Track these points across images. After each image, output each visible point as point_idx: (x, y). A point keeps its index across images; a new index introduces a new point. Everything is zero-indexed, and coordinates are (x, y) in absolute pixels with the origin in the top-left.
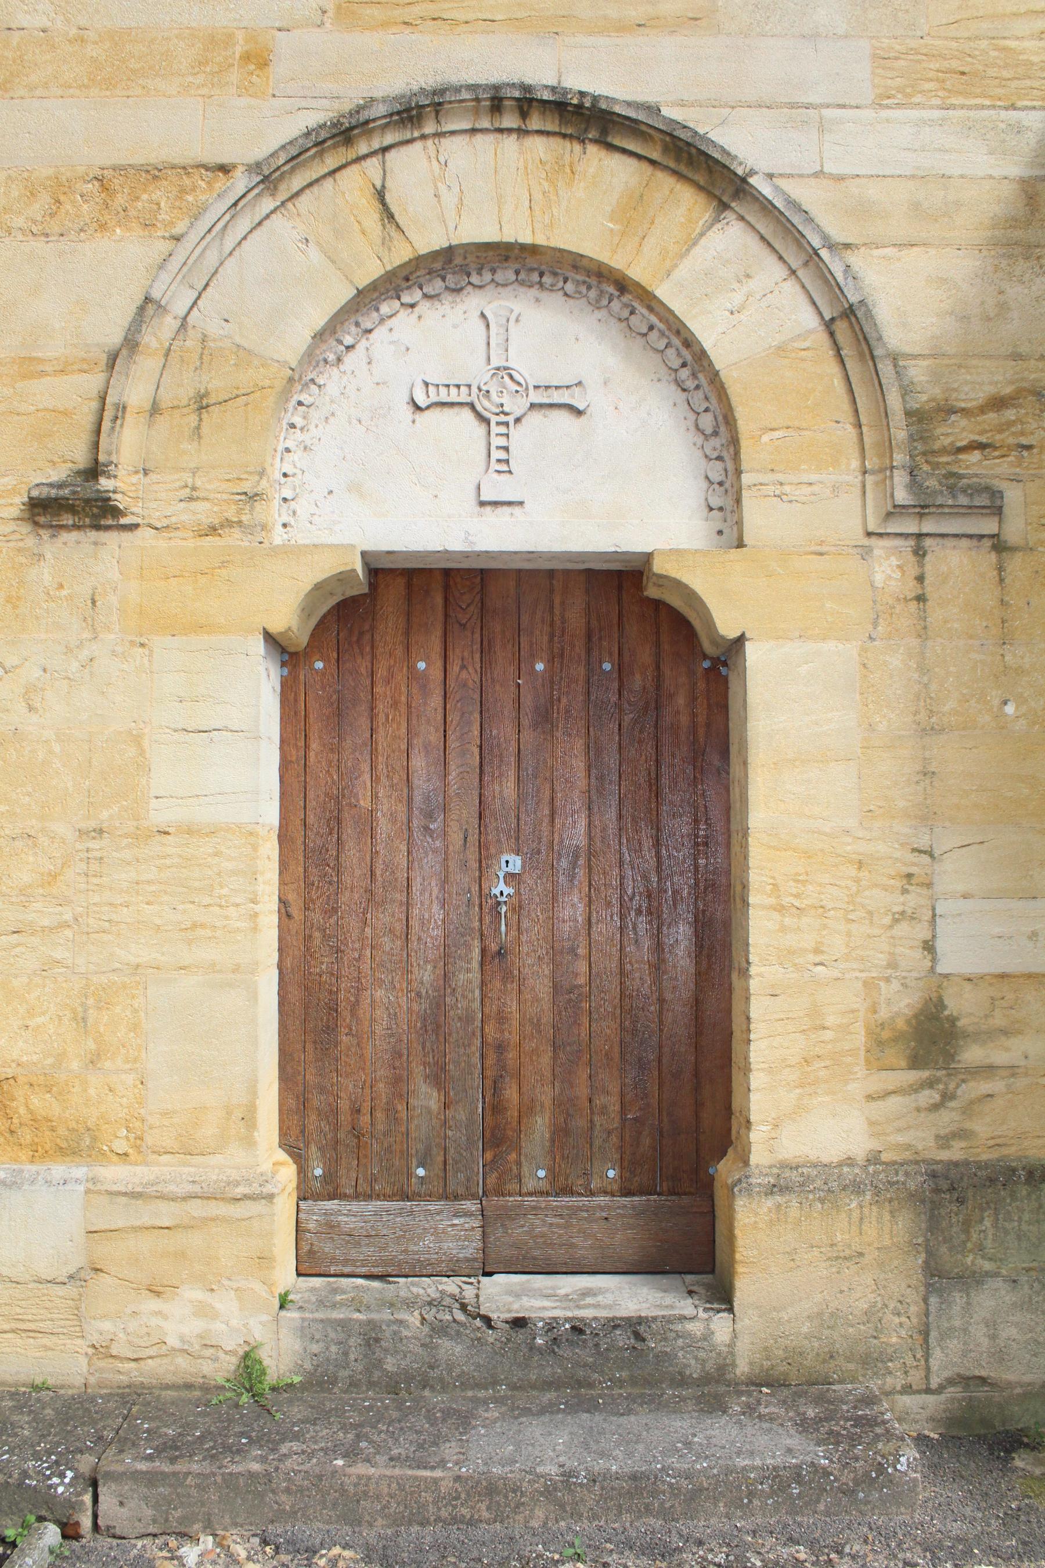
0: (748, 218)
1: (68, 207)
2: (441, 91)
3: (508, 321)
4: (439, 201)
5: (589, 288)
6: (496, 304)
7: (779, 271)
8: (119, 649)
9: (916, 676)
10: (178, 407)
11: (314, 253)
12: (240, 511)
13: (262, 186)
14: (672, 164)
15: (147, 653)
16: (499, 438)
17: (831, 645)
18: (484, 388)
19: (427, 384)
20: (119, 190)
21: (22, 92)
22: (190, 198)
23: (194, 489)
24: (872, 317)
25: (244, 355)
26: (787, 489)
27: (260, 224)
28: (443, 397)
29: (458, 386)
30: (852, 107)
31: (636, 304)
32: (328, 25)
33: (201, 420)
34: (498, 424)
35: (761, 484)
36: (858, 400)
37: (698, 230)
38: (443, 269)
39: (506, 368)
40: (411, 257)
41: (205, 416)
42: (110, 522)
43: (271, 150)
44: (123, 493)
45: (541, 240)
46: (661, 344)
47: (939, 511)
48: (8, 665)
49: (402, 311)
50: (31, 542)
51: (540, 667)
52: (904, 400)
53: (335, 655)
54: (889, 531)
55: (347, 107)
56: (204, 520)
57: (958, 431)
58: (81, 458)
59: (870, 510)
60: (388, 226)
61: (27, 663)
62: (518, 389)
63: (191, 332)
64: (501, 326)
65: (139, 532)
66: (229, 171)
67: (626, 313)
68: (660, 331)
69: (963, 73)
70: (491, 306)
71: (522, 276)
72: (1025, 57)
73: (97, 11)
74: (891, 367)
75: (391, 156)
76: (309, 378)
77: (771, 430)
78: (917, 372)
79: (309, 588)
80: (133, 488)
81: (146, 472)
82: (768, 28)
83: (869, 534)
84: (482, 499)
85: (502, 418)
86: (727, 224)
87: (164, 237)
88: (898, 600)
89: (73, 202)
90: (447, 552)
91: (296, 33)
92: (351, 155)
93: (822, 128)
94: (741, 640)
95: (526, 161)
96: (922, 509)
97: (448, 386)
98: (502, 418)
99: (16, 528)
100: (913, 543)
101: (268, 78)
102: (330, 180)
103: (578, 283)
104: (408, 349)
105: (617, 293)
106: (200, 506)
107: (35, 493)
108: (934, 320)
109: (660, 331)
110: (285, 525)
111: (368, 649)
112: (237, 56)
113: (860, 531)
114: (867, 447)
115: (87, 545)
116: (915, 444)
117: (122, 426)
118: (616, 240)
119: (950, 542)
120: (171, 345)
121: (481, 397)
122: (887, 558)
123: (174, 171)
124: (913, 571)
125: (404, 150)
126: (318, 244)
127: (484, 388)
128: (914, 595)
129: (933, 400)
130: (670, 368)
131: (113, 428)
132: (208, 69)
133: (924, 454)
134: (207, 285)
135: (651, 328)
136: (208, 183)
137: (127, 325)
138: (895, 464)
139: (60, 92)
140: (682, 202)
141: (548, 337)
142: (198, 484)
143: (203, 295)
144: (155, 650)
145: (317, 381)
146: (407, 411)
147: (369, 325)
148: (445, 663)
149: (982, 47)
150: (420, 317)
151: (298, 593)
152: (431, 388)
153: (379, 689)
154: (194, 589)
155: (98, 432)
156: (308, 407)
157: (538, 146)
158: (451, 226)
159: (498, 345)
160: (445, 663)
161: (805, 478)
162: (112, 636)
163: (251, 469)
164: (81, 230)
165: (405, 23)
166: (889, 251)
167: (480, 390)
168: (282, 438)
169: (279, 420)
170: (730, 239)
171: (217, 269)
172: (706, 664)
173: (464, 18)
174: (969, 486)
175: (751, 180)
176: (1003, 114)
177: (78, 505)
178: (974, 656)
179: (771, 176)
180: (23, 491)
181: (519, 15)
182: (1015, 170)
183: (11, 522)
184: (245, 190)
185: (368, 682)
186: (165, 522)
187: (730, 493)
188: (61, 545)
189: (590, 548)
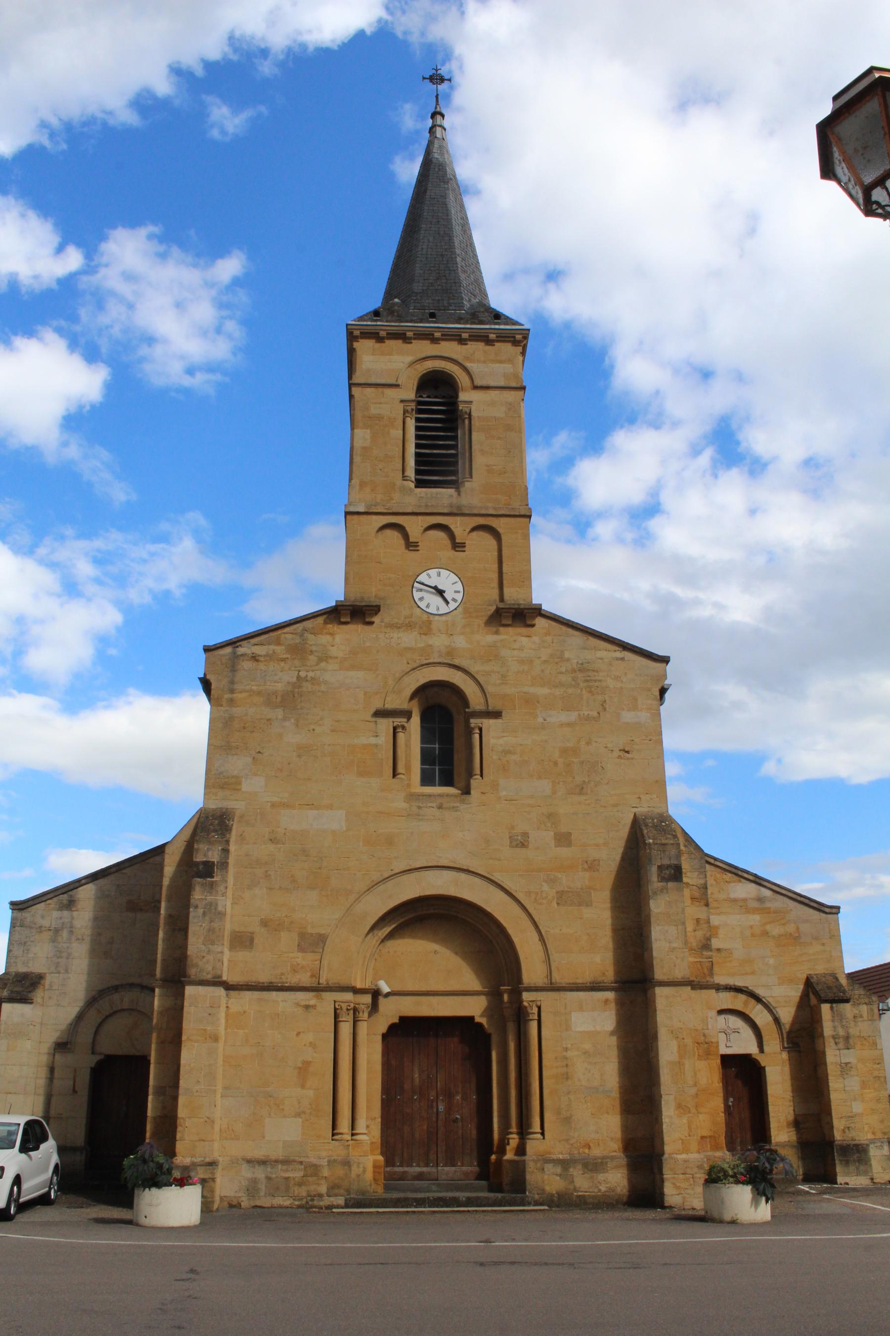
140: (753, 1002)
141: (735, 1022)
170: (759, 1007)
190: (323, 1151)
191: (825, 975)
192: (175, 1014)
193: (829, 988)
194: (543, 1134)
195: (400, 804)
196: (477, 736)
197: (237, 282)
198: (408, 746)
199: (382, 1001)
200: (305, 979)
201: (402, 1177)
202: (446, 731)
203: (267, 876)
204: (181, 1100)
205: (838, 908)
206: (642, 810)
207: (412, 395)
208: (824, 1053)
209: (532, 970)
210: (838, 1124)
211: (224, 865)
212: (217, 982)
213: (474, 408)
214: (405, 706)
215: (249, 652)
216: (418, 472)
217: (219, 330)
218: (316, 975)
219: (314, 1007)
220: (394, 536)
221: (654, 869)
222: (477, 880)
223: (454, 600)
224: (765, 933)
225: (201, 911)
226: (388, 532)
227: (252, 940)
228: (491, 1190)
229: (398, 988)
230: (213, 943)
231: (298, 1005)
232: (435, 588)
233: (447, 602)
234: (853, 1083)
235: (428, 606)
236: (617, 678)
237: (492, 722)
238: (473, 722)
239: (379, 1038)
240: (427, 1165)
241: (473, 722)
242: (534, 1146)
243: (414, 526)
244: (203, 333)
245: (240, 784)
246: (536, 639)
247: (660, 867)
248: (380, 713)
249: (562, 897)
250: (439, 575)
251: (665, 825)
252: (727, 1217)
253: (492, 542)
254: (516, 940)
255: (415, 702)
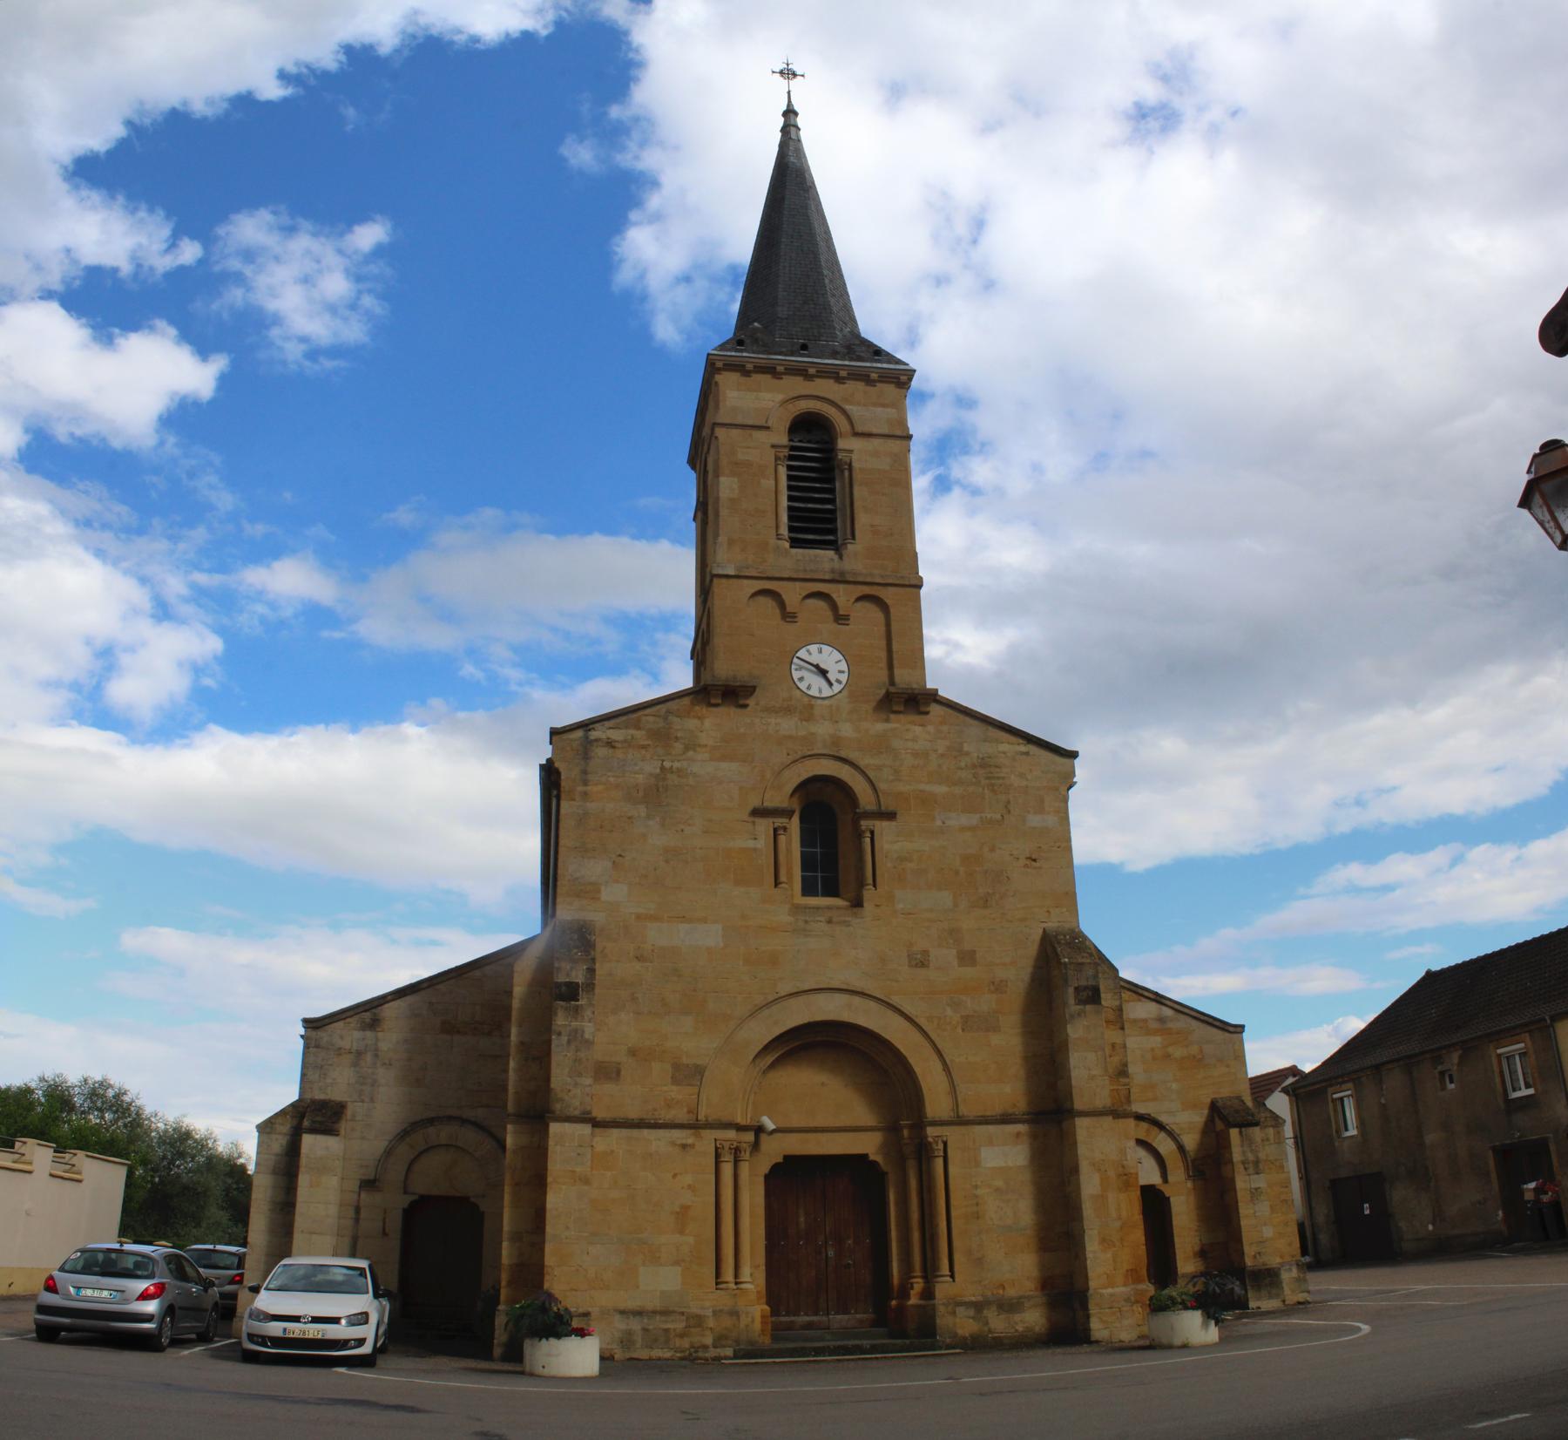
170: (1163, 1135)
190: (706, 1301)
191: (1230, 1098)
192: (537, 1156)
193: (1237, 1112)
194: (952, 1276)
195: (783, 916)
196: (868, 840)
197: (379, 252)
198: (789, 851)
199: (763, 1137)
200: (681, 1115)
201: (790, 1327)
202: (829, 835)
203: (634, 999)
204: (548, 1248)
205: (1243, 1027)
206: (1052, 925)
207: (784, 440)
208: (1233, 1180)
209: (936, 1103)
210: (1249, 1250)
211: (590, 986)
212: (586, 1118)
213: (854, 457)
214: (785, 805)
215: (604, 736)
216: (791, 529)
217: (353, 307)
218: (693, 1111)
219: (692, 1146)
220: (768, 603)
221: (1071, 991)
222: (872, 1004)
223: (839, 681)
224: (1167, 1056)
225: (565, 1039)
226: (761, 599)
227: (618, 1073)
228: (891, 1336)
229: (783, 1125)
230: (580, 1075)
231: (673, 1144)
232: (817, 666)
233: (830, 684)
234: (1263, 1208)
235: (809, 687)
236: (1022, 775)
237: (885, 824)
238: (864, 824)
239: (762, 1179)
240: (816, 1314)
241: (864, 824)
242: (943, 1289)
243: (792, 594)
244: (332, 309)
245: (599, 891)
246: (931, 728)
247: (1076, 989)
248: (759, 813)
249: (967, 1022)
250: (820, 651)
251: (1079, 943)
252: (1177, 1342)
253: (880, 616)
254: (917, 1070)
255: (795, 800)
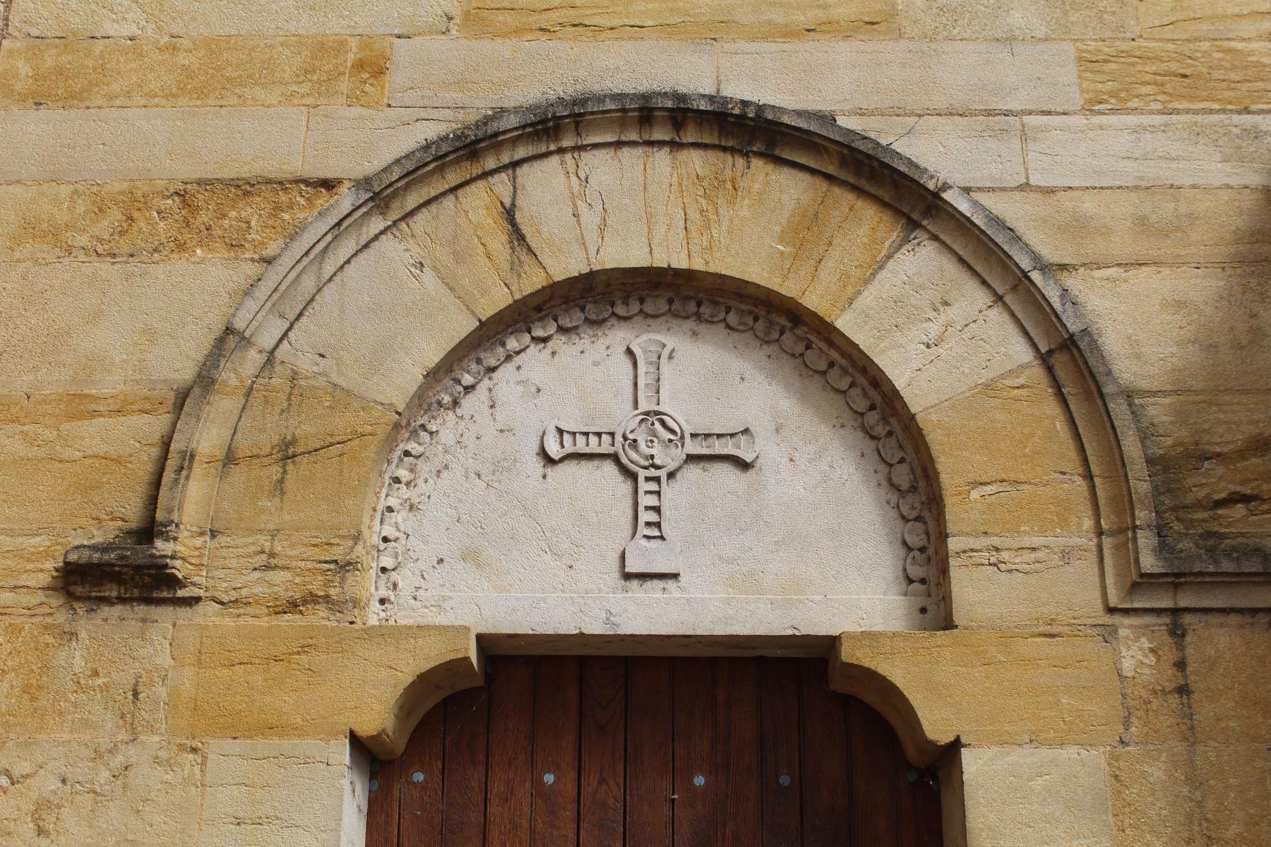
0: (942, 237)
1: (142, 225)
2: (584, 101)
3: (659, 358)
4: (578, 222)
5: (756, 319)
6: (645, 337)
7: (981, 297)
8: (163, 754)
9: (1185, 790)
10: (258, 456)
11: (429, 279)
12: (327, 584)
13: (371, 204)
14: (851, 179)
15: (199, 761)
16: (649, 496)
17: (1071, 752)
18: (631, 436)
19: (561, 432)
20: (203, 207)
21: (100, 102)
22: (286, 217)
23: (272, 555)
24: (1098, 349)
25: (342, 397)
26: (1005, 555)
27: (366, 246)
28: (581, 446)
29: (599, 435)
30: (1058, 114)
31: (812, 338)
32: (454, 32)
33: (285, 472)
34: (648, 479)
35: (972, 550)
36: (1087, 446)
37: (884, 252)
38: (582, 298)
39: (657, 413)
40: (545, 284)
41: (290, 467)
42: (165, 594)
43: (384, 164)
44: (183, 559)
45: (698, 265)
46: (844, 384)
47: (1200, 581)
48: (16, 773)
49: (532, 346)
50: (61, 617)
51: (699, 781)
52: (1144, 446)
53: (440, 765)
54: (1136, 605)
55: (473, 117)
56: (282, 593)
57: (1213, 481)
58: (131, 510)
59: (1110, 581)
60: (518, 249)
61: (42, 772)
62: (672, 437)
63: (278, 368)
64: (651, 363)
65: (200, 608)
66: (333, 187)
67: (800, 348)
68: (841, 367)
69: (1185, 76)
70: (639, 340)
71: (677, 305)
72: (1254, 59)
73: (194, 19)
74: (1125, 407)
75: (523, 171)
76: (418, 423)
77: (981, 484)
78: (1158, 411)
79: (410, 680)
80: (197, 553)
81: (214, 534)
82: (956, 31)
83: (1111, 611)
84: (627, 570)
85: (653, 472)
86: (919, 244)
87: (252, 260)
88: (1155, 692)
89: (148, 220)
90: (582, 634)
91: (418, 40)
92: (477, 170)
93: (1024, 136)
94: (956, 745)
95: (680, 177)
96: (1175, 580)
97: (586, 434)
98: (653, 472)
99: (44, 599)
100: (1168, 621)
101: (383, 87)
102: (451, 197)
103: (741, 313)
104: (539, 390)
105: (789, 325)
106: (279, 577)
107: (73, 557)
108: (1174, 350)
109: (841, 367)
110: (382, 601)
111: (481, 757)
112: (349, 64)
113: (1099, 605)
114: (1101, 502)
115: (133, 622)
116: (1162, 498)
117: (187, 478)
118: (787, 264)
119: (1214, 619)
120: (254, 382)
121: (627, 447)
122: (1137, 639)
123: (269, 186)
124: (1170, 655)
125: (538, 166)
126: (435, 269)
127: (631, 436)
128: (1174, 685)
129: (1180, 444)
130: (855, 412)
131: (176, 481)
132: (315, 77)
133: (1173, 509)
134: (301, 314)
135: (831, 365)
136: (308, 199)
137: (201, 358)
138: (1138, 523)
139: (143, 102)
140: (863, 223)
141: (707, 380)
142: (278, 549)
143: (296, 326)
144: (210, 756)
145: (429, 427)
146: (536, 465)
147: (493, 363)
148: (579, 775)
149: (1204, 48)
150: (553, 353)
151: (395, 686)
152: (566, 437)
153: (493, 809)
154: (265, 680)
155: (157, 483)
156: (417, 457)
157: (695, 161)
158: (592, 250)
159: (647, 385)
160: (579, 775)
161: (1027, 541)
162: (157, 738)
163: (343, 532)
164: (156, 250)
165: (541, 30)
166: (1113, 272)
167: (625, 438)
168: (383, 495)
169: (381, 474)
170: (921, 262)
171: (314, 296)
172: (912, 777)
173: (609, 24)
174: (1234, 549)
175: (945, 196)
176: (1236, 118)
177: (124, 574)
178: (1260, 763)
179: (967, 190)
180: (57, 554)
181: (671, 21)
182: (1256, 180)
183: (40, 592)
184: (351, 208)
185: (481, 798)
186: (234, 595)
187: (933, 562)
188: (99, 622)
189: (761, 631)
